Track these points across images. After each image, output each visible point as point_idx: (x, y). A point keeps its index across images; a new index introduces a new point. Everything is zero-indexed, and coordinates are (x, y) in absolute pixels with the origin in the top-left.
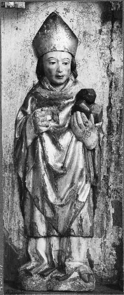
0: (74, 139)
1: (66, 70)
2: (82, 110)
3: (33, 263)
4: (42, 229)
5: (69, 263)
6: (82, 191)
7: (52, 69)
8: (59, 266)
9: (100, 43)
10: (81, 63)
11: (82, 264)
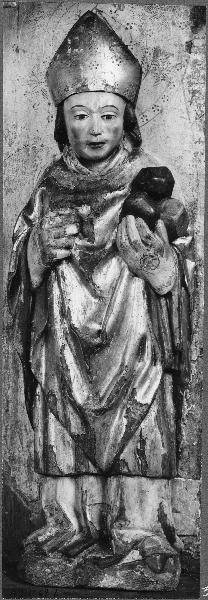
0: (127, 273)
1: (109, 130)
2: (138, 213)
3: (50, 531)
4: (66, 459)
5: (121, 532)
6: (143, 382)
7: (79, 130)
8: (101, 538)
9: (189, 71)
10: (150, 115)
11: (149, 534)
